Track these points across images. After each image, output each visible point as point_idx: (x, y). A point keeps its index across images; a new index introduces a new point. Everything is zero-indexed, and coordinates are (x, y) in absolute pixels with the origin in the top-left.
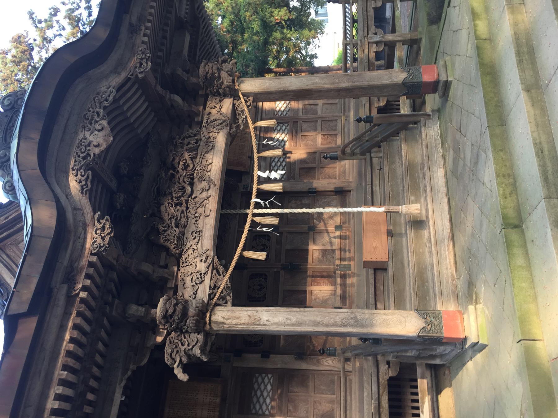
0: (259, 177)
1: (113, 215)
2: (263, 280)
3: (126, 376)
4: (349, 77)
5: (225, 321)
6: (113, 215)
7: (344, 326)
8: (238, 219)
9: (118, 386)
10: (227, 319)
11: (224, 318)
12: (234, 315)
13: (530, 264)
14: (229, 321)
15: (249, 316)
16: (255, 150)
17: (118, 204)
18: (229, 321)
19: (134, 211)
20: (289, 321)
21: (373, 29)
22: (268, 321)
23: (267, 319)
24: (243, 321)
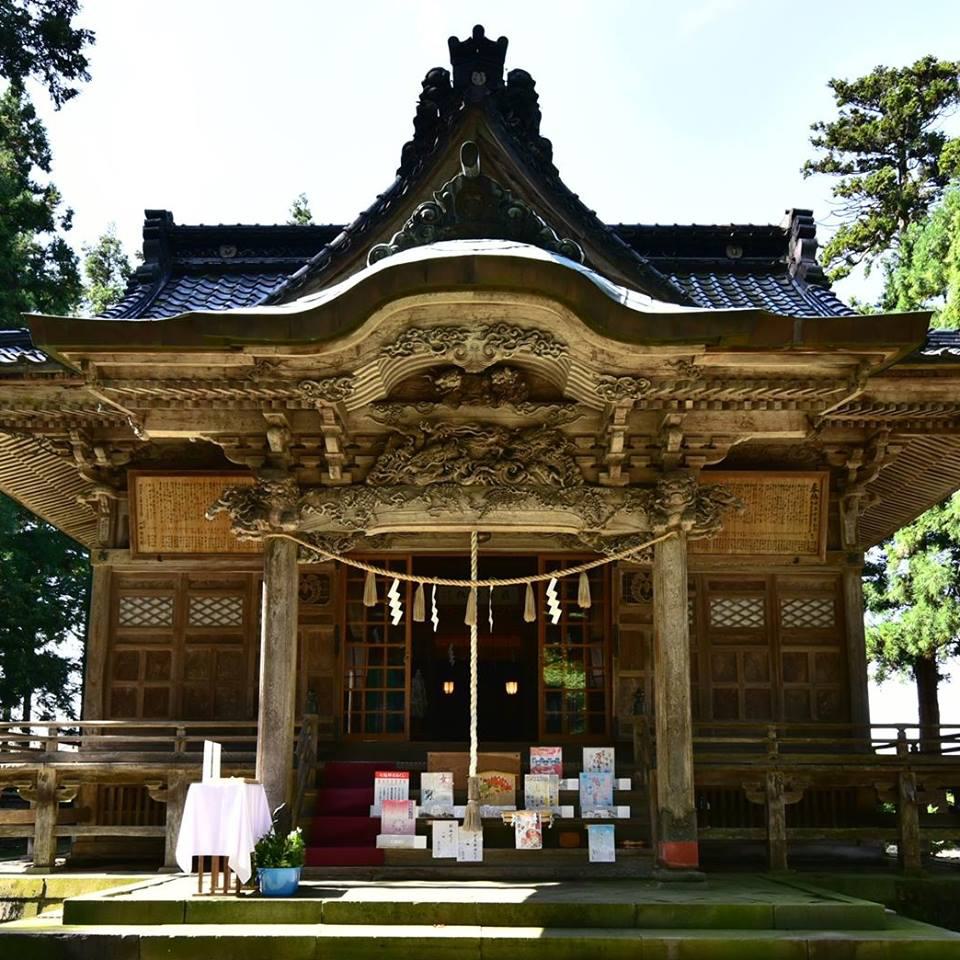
0: (547, 583)
1: (427, 376)
2: (318, 598)
3: (212, 440)
4: (680, 722)
5: (275, 557)
6: (427, 376)
7: (267, 714)
8: (562, 550)
9: (199, 432)
10: (276, 560)
11: (278, 556)
12: (283, 568)
13: (193, 643)
14: (274, 563)
15: (280, 590)
16: (379, 572)
17: (441, 381)
18: (274, 563)
19: (437, 405)
20: (273, 642)
21: (546, 690)
22: (275, 613)
23: (277, 612)
24: (274, 581)
